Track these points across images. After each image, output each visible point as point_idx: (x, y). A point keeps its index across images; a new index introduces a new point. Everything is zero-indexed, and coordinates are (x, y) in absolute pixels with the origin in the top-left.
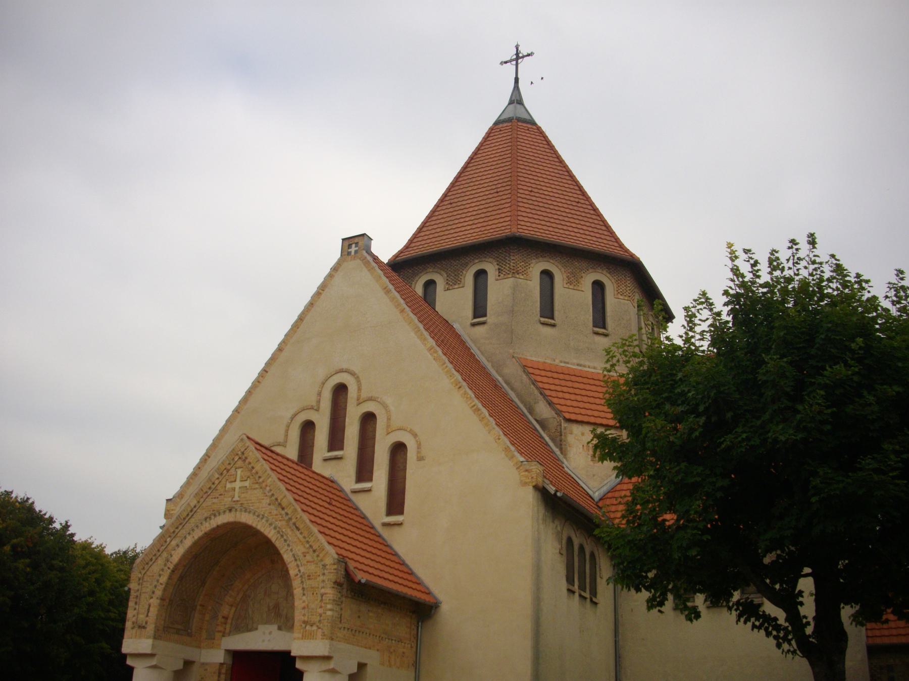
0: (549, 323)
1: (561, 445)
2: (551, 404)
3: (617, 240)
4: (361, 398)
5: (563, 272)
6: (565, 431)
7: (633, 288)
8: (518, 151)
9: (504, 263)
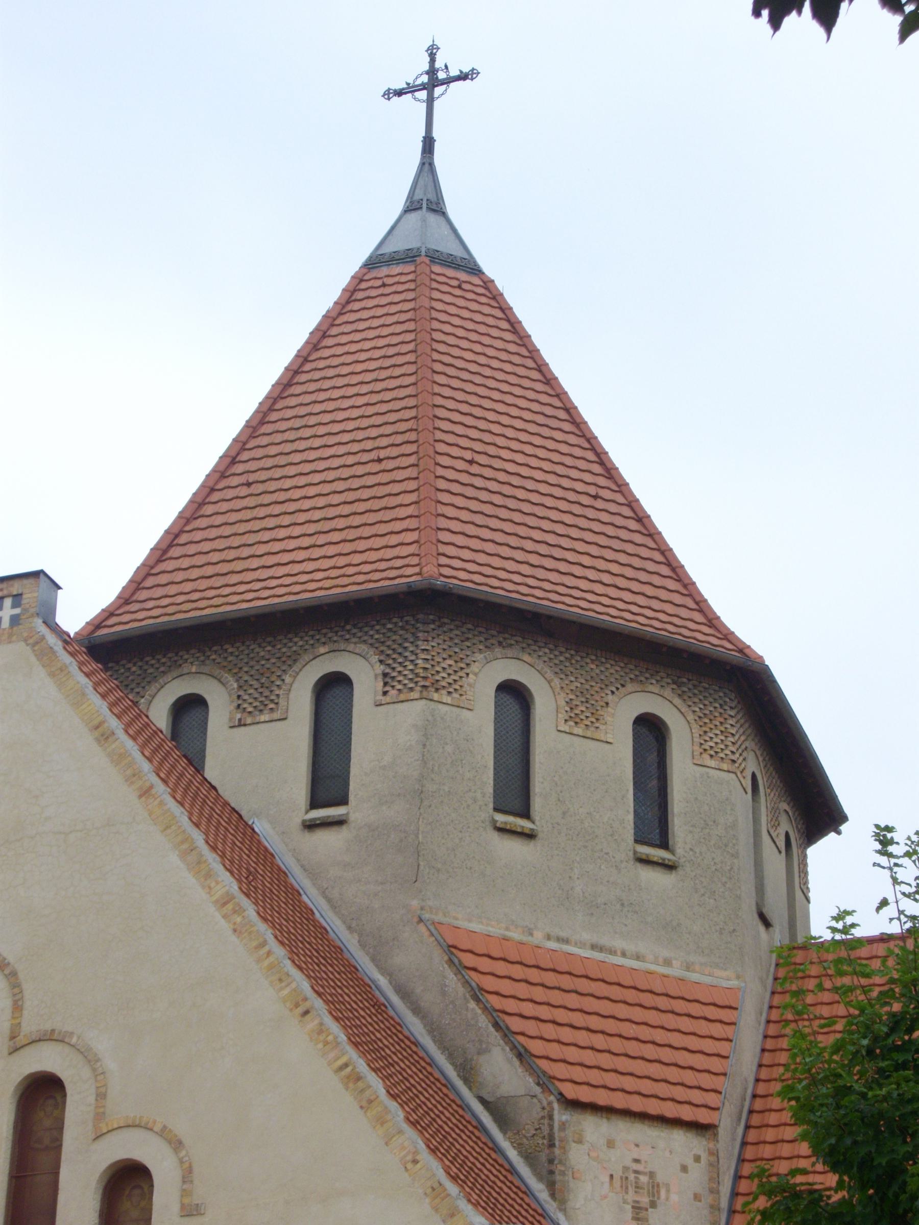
0: (519, 830)
1: (551, 1172)
2: (523, 1056)
3: (701, 605)
4: (22, 1034)
5: (558, 690)
6: (562, 1134)
7: (743, 738)
8: (436, 346)
9: (400, 660)
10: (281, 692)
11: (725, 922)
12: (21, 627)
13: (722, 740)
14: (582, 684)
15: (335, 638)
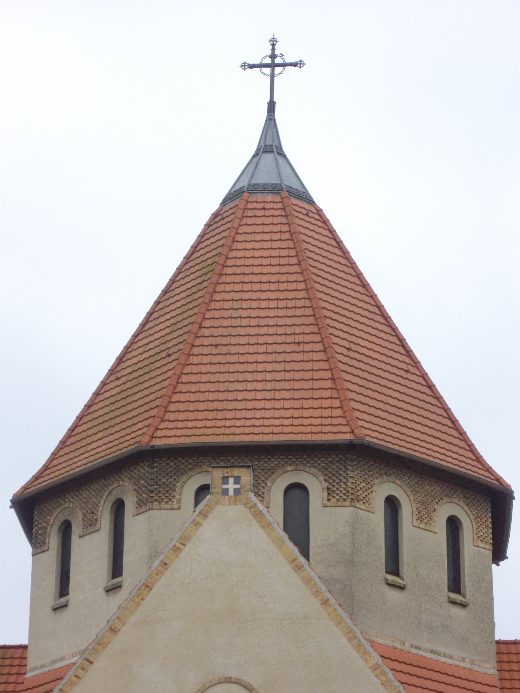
0: (398, 585)
9: (338, 481)
10: (265, 491)
11: (488, 637)
12: (241, 496)
13: (486, 531)
14: (423, 497)
15: (297, 462)
